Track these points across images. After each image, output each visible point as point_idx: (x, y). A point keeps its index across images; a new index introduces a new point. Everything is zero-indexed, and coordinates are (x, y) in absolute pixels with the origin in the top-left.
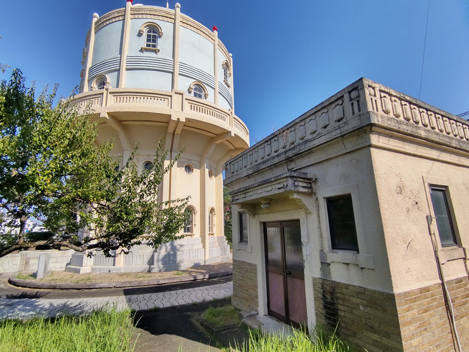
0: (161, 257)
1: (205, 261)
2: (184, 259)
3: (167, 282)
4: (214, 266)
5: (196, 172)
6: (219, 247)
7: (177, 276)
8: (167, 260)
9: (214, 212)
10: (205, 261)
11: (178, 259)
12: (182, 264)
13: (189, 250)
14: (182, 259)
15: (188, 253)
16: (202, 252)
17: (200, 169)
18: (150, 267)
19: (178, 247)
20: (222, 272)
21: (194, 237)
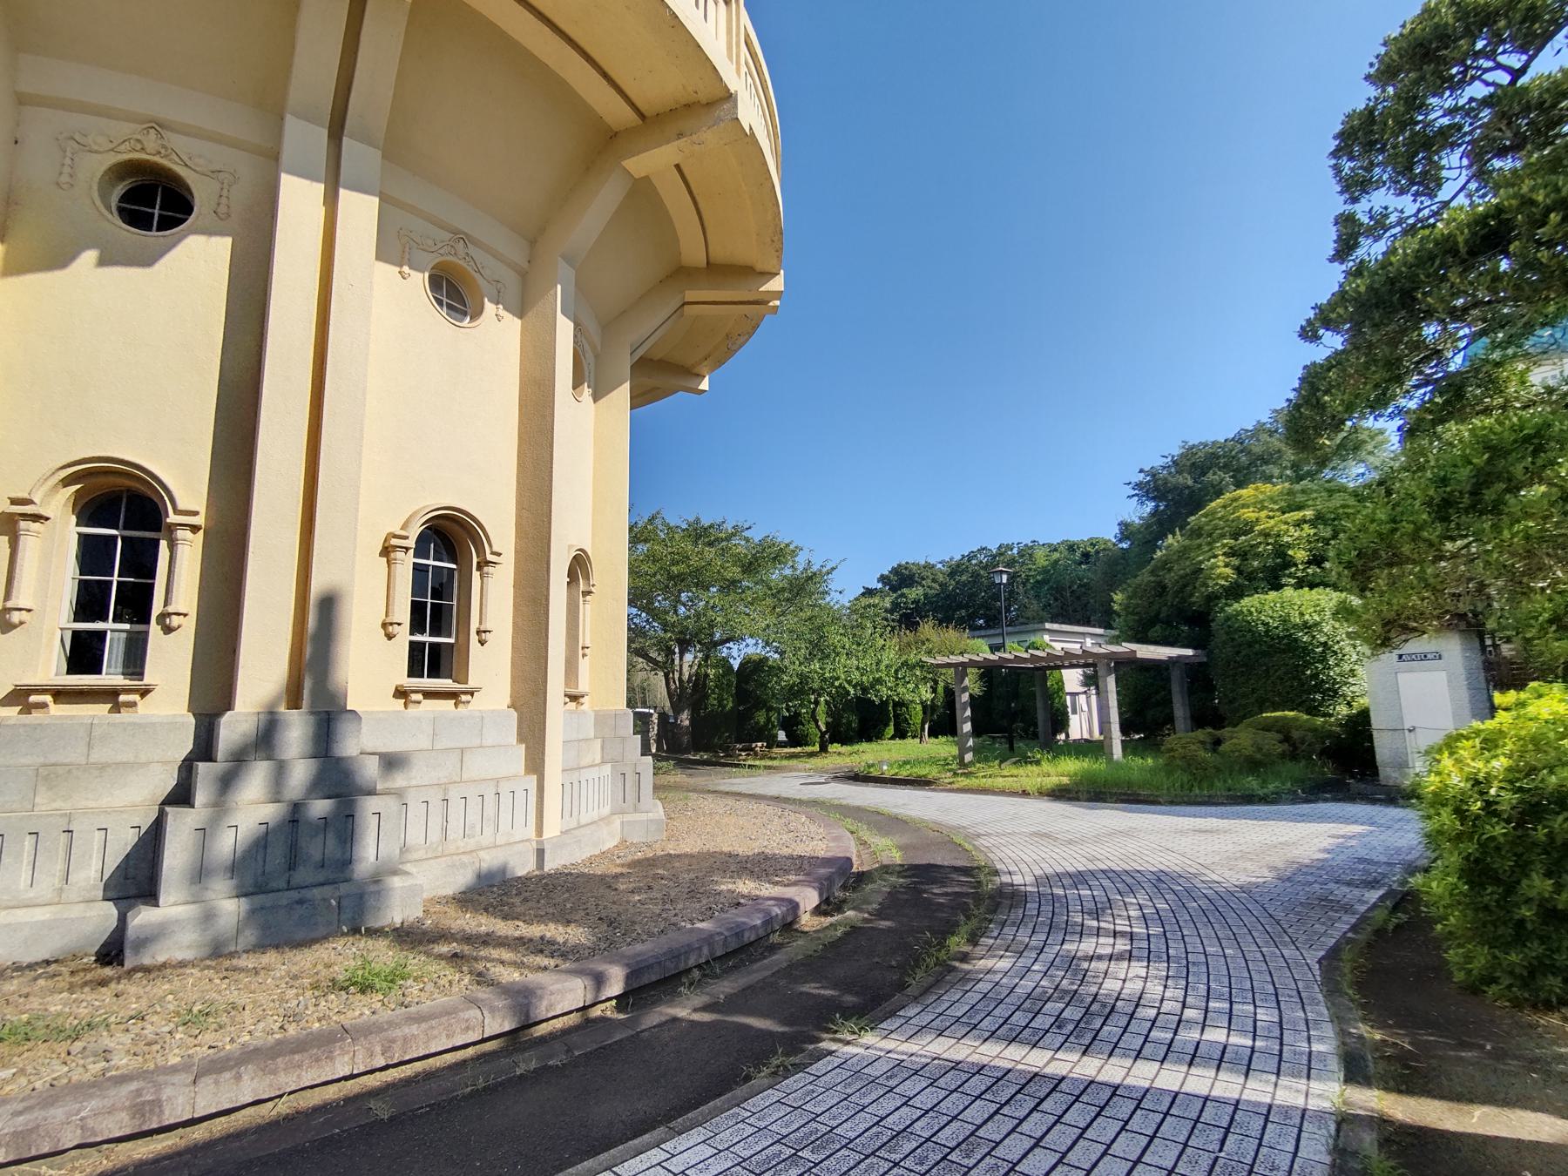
0: (227, 843)
1: (540, 853)
2: (404, 849)
3: (248, 1087)
4: (607, 882)
5: (499, 331)
6: (607, 769)
7: (361, 1009)
8: (277, 857)
9: (587, 578)
10: (540, 853)
11: (369, 852)
12: (396, 882)
13: (444, 787)
14: (390, 849)
15: (435, 802)
16: (520, 795)
17: (520, 317)
18: (122, 920)
19: (370, 770)
20: (709, 939)
21: (477, 704)
